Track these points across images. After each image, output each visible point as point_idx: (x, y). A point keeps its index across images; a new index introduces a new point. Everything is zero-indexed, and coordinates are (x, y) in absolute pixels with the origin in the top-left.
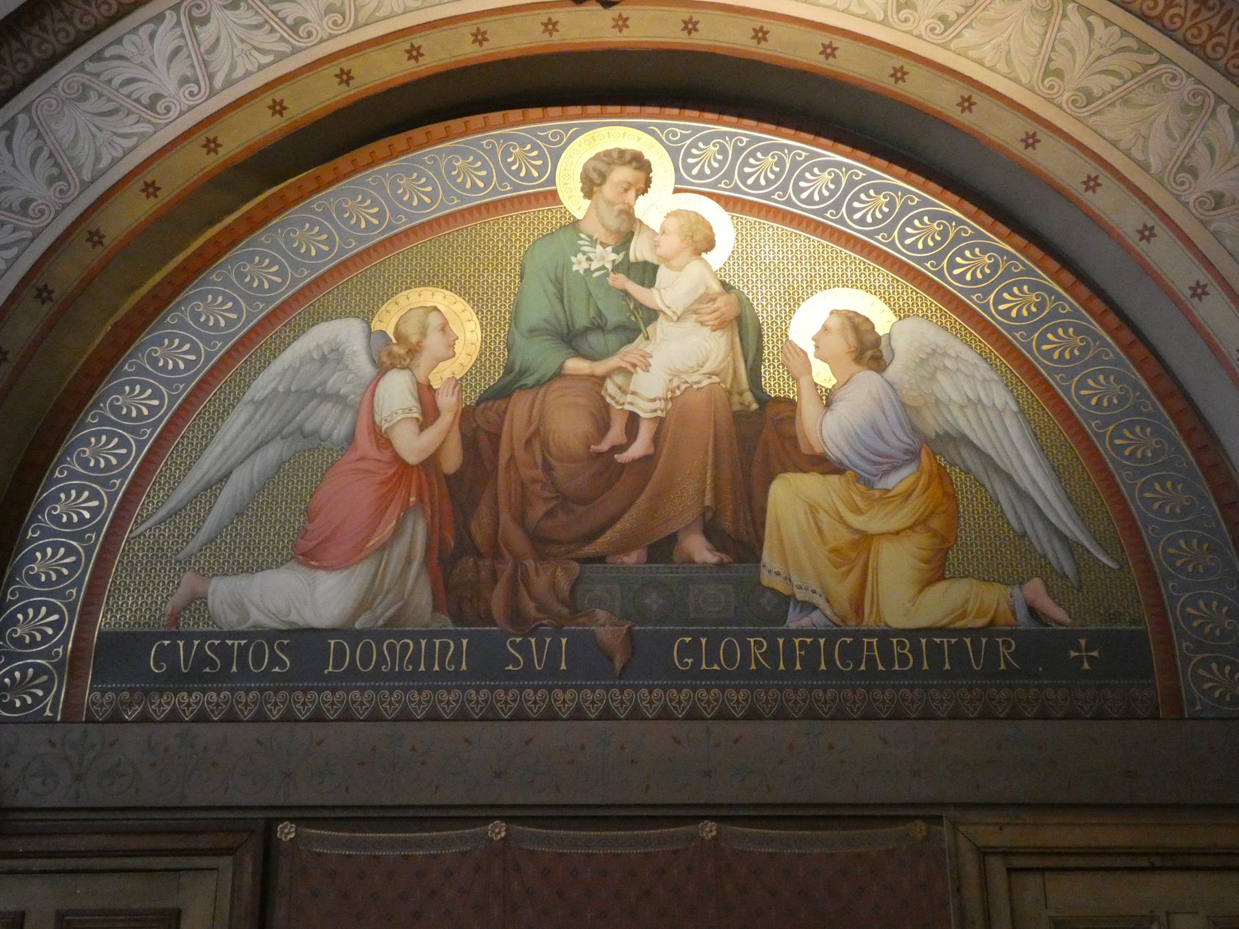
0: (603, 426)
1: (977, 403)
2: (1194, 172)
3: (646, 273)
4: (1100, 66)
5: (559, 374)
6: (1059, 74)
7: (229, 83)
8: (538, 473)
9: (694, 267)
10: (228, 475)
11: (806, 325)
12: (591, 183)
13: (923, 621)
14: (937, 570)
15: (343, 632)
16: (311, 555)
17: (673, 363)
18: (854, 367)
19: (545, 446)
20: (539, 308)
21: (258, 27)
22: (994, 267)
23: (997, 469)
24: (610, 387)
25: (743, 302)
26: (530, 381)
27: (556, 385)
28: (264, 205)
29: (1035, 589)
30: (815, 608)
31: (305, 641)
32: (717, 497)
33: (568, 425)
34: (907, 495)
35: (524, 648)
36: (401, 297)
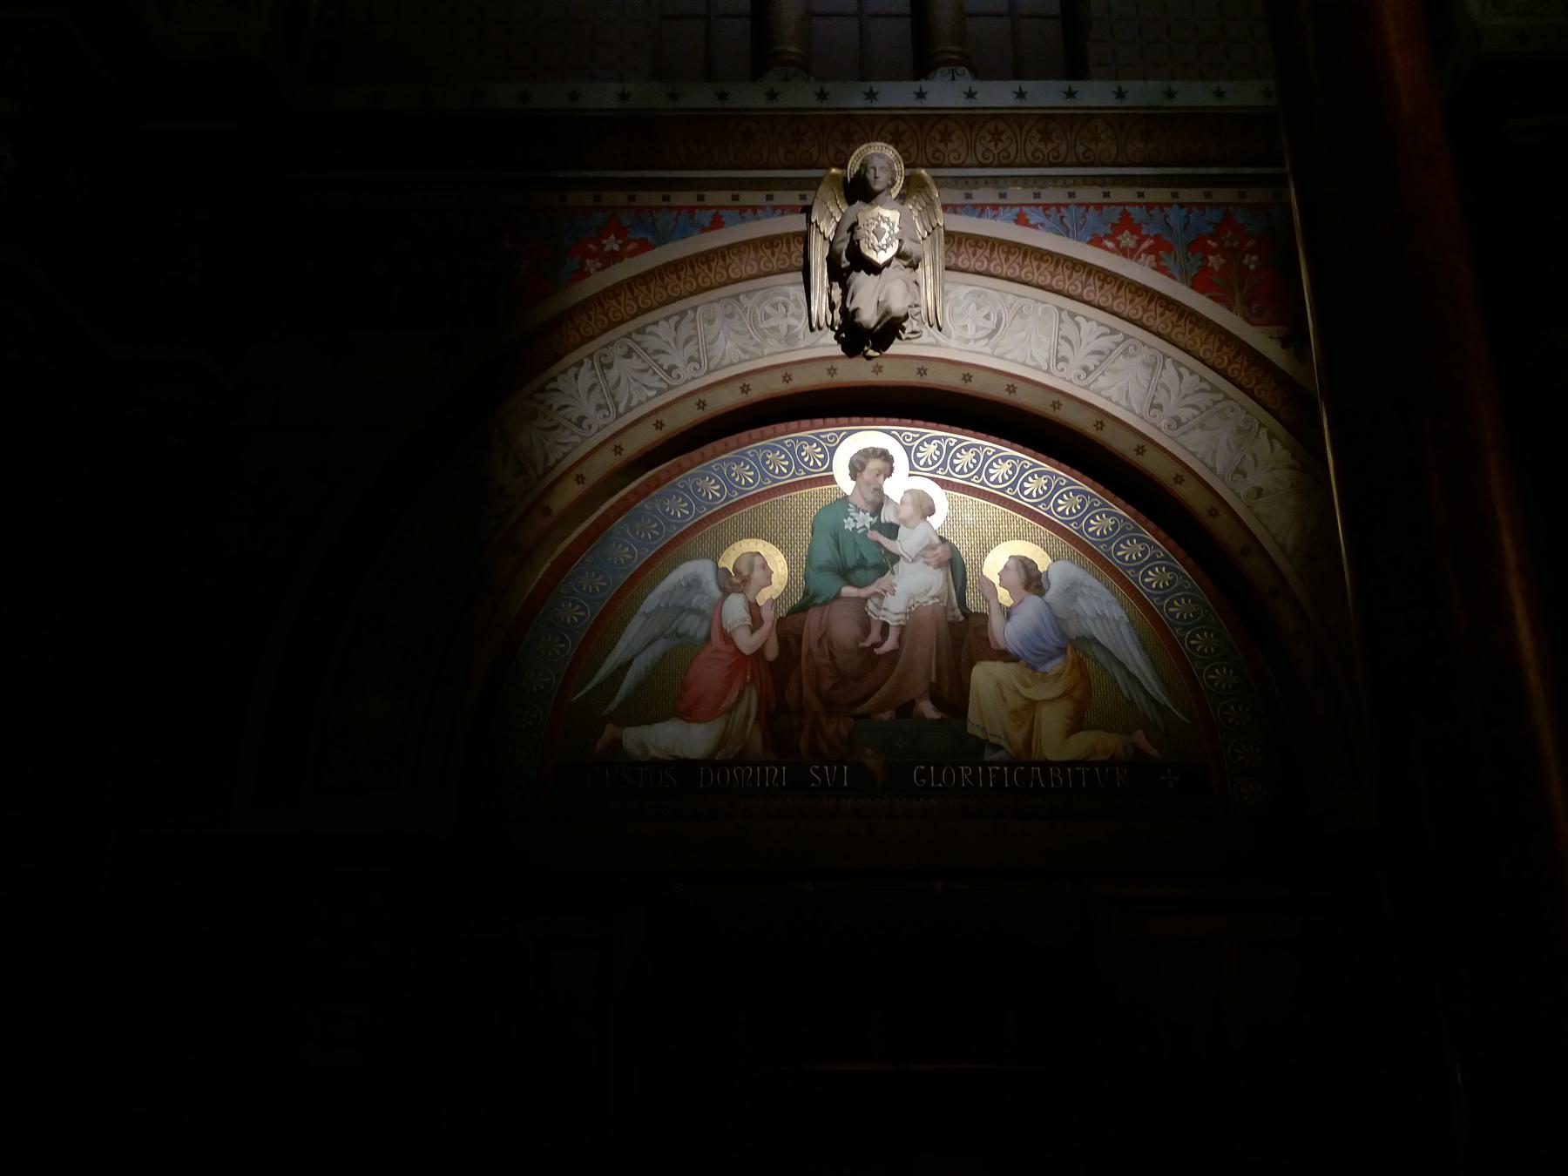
0: (866, 630)
1: (1103, 617)
2: (1244, 475)
3: (892, 531)
4: (1188, 401)
5: (838, 596)
6: (1159, 407)
7: (629, 409)
8: (827, 661)
9: (922, 526)
10: (630, 662)
11: (994, 564)
12: (856, 469)
13: (1068, 756)
14: (1077, 723)
15: (708, 762)
16: (687, 714)
17: (911, 587)
18: (1024, 593)
19: (830, 643)
20: (825, 554)
21: (646, 371)
22: (1115, 527)
23: (1114, 658)
24: (870, 605)
25: (954, 549)
26: (819, 601)
27: (837, 603)
28: (646, 483)
29: (1139, 736)
30: (1001, 748)
31: (683, 767)
32: (938, 674)
33: (844, 630)
34: (1058, 676)
35: (821, 772)
36: (736, 545)
